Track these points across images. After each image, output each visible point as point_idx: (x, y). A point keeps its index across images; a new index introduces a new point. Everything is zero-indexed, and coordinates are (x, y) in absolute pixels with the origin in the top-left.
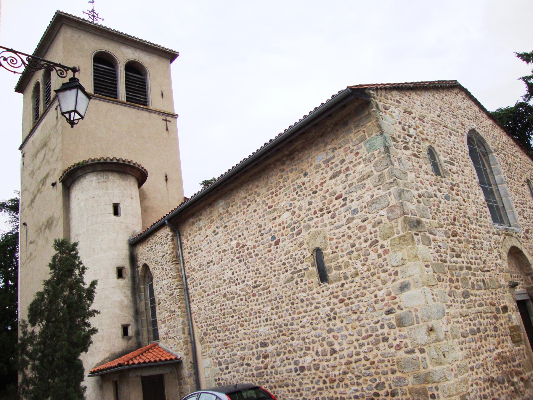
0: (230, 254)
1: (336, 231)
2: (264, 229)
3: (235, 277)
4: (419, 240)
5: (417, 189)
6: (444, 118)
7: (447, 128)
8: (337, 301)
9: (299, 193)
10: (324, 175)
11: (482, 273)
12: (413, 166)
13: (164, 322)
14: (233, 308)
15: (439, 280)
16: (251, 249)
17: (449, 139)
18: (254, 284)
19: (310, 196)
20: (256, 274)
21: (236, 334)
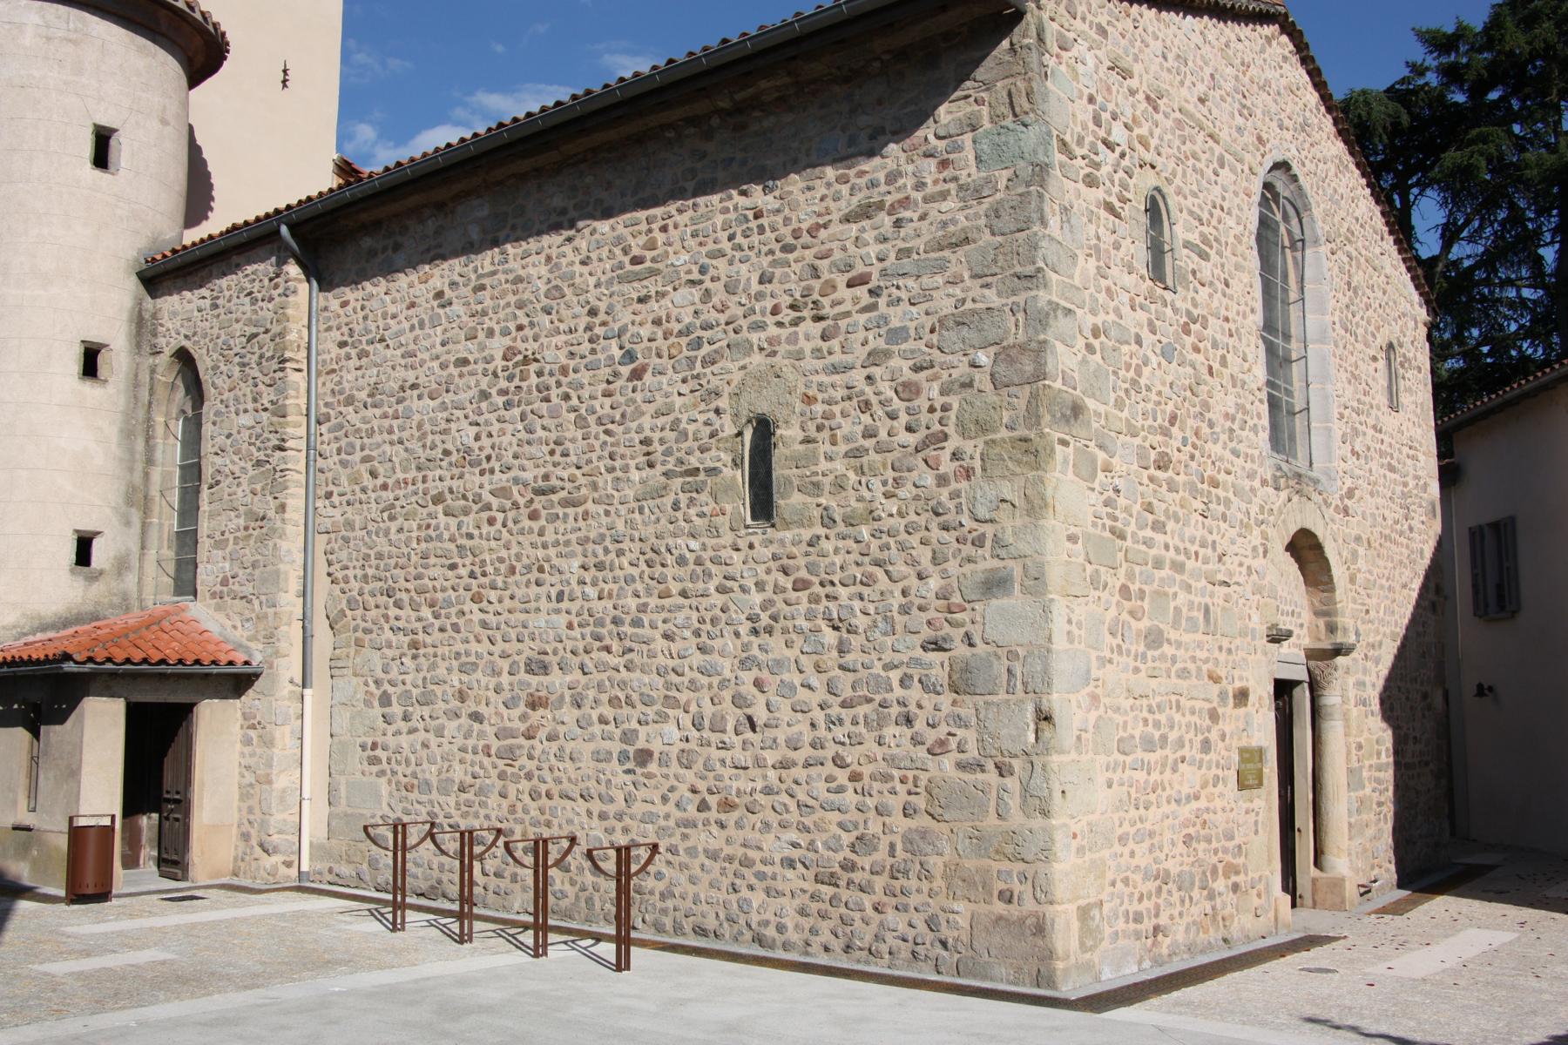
0: (480, 376)
1: (826, 379)
2: (604, 324)
3: (481, 449)
4: (1065, 461)
5: (1093, 312)
6: (1215, 111)
7: (1217, 142)
8: (787, 583)
9: (739, 239)
10: (829, 202)
11: (1210, 587)
12: (1098, 238)
13: (220, 545)
14: (460, 541)
15: (1095, 582)
16: (551, 374)
17: (1214, 178)
18: (540, 483)
19: (770, 258)
20: (552, 453)
21: (454, 619)
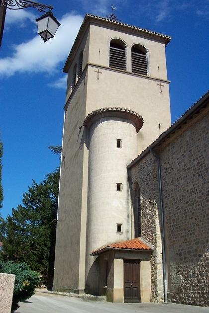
3: (195, 188)
21: (193, 231)
